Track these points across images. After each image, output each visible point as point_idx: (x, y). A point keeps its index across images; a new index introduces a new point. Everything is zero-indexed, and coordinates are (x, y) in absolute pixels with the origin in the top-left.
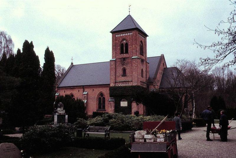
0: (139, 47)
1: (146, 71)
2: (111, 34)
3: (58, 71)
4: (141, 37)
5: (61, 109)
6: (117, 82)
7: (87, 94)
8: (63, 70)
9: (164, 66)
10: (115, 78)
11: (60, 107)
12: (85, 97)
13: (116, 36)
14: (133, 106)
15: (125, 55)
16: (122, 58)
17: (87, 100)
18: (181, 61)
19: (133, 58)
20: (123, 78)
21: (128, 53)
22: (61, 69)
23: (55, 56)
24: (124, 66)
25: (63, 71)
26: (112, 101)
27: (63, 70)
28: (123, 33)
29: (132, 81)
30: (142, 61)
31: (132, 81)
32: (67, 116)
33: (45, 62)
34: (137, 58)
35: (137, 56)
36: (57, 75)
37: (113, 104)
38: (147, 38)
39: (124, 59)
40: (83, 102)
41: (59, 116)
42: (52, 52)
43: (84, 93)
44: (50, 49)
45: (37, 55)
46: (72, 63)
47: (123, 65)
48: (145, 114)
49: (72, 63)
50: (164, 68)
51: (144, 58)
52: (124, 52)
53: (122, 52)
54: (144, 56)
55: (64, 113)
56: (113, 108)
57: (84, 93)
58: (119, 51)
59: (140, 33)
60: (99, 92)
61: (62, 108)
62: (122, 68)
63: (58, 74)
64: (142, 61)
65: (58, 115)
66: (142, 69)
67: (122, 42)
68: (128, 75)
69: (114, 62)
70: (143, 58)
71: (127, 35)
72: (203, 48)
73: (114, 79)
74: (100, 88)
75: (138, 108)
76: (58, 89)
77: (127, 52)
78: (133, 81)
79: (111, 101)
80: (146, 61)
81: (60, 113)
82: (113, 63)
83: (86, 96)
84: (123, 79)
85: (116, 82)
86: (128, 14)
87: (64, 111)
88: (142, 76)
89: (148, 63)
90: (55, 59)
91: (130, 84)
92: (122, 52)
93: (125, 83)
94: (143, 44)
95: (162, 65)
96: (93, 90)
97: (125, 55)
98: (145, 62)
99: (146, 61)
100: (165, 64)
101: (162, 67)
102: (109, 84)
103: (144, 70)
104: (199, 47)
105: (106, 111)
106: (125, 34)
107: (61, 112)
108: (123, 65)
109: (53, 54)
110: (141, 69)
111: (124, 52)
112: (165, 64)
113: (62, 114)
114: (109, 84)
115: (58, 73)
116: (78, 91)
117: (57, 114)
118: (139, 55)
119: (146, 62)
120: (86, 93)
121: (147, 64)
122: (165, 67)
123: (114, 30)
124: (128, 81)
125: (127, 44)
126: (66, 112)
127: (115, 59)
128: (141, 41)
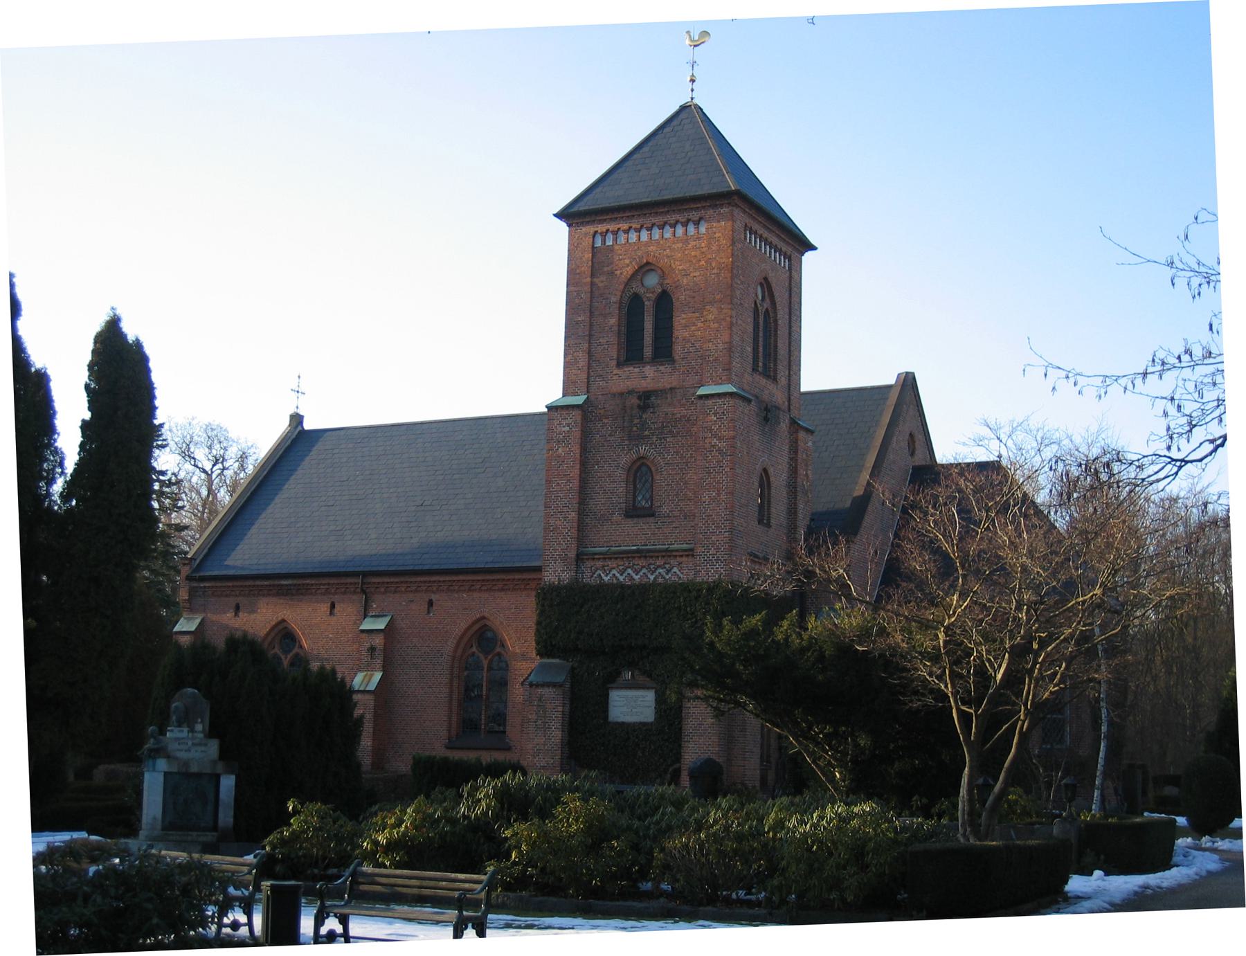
0: (750, 320)
1: (793, 487)
2: (562, 228)
3: (208, 467)
4: (769, 258)
5: (192, 730)
6: (593, 556)
7: (388, 631)
8: (243, 458)
9: (912, 454)
10: (581, 526)
11: (186, 720)
12: (372, 649)
13: (598, 243)
14: (690, 725)
15: (649, 376)
16: (630, 392)
17: (385, 670)
18: (1007, 430)
19: (701, 397)
20: (631, 526)
21: (673, 361)
22: (232, 453)
23: (158, 376)
24: (643, 450)
25: (242, 468)
26: (554, 685)
27: (243, 458)
28: (678, 217)
29: (690, 553)
30: (768, 414)
31: (690, 553)
32: (228, 783)
33: (87, 415)
34: (731, 394)
35: (729, 381)
36: (204, 492)
37: (555, 705)
38: (808, 257)
39: (646, 399)
40: (342, 694)
41: (172, 785)
42: (138, 345)
43: (368, 625)
44: (131, 330)
45: (131, 338)
46: (297, 419)
47: (635, 438)
48: (771, 776)
49: (297, 419)
50: (914, 468)
51: (779, 397)
52: (648, 351)
53: (631, 354)
54: (783, 381)
55: (214, 762)
56: (556, 734)
57: (368, 625)
58: (609, 345)
59: (756, 226)
60: (470, 621)
61: (199, 727)
62: (625, 460)
63: (210, 491)
64: (768, 414)
65: (166, 774)
66: (765, 470)
67: (636, 287)
68: (665, 509)
69: (577, 415)
70: (775, 394)
71: (668, 235)
72: (1090, 393)
73: (574, 533)
74: (476, 595)
75: (729, 741)
76: (193, 592)
77: (664, 351)
78: (699, 550)
79: (544, 685)
80: (794, 413)
81: (186, 764)
82: (569, 427)
83: (378, 641)
84: (631, 534)
85: (580, 558)
86: (685, 100)
87: (213, 747)
88: (764, 517)
89: (807, 430)
90: (157, 393)
91: (679, 573)
92: (631, 354)
93: (642, 562)
94: (773, 303)
95: (900, 442)
96: (431, 603)
97: (649, 370)
98: (784, 426)
99: (794, 413)
100: (920, 436)
101: (900, 460)
102: (539, 569)
103: (779, 479)
104: (1066, 388)
105: (509, 749)
106: (691, 228)
107: (196, 754)
108: (635, 438)
109: (144, 359)
110: (759, 468)
111: (648, 351)
112: (919, 437)
113: (194, 769)
114: (539, 569)
115: (209, 475)
116: (325, 607)
117: (162, 764)
118: (747, 377)
119: (793, 422)
120: (381, 624)
121: (802, 434)
122: (919, 459)
123: (582, 207)
124: (668, 553)
125: (664, 301)
126: (224, 755)
127: (580, 400)
128: (766, 284)
